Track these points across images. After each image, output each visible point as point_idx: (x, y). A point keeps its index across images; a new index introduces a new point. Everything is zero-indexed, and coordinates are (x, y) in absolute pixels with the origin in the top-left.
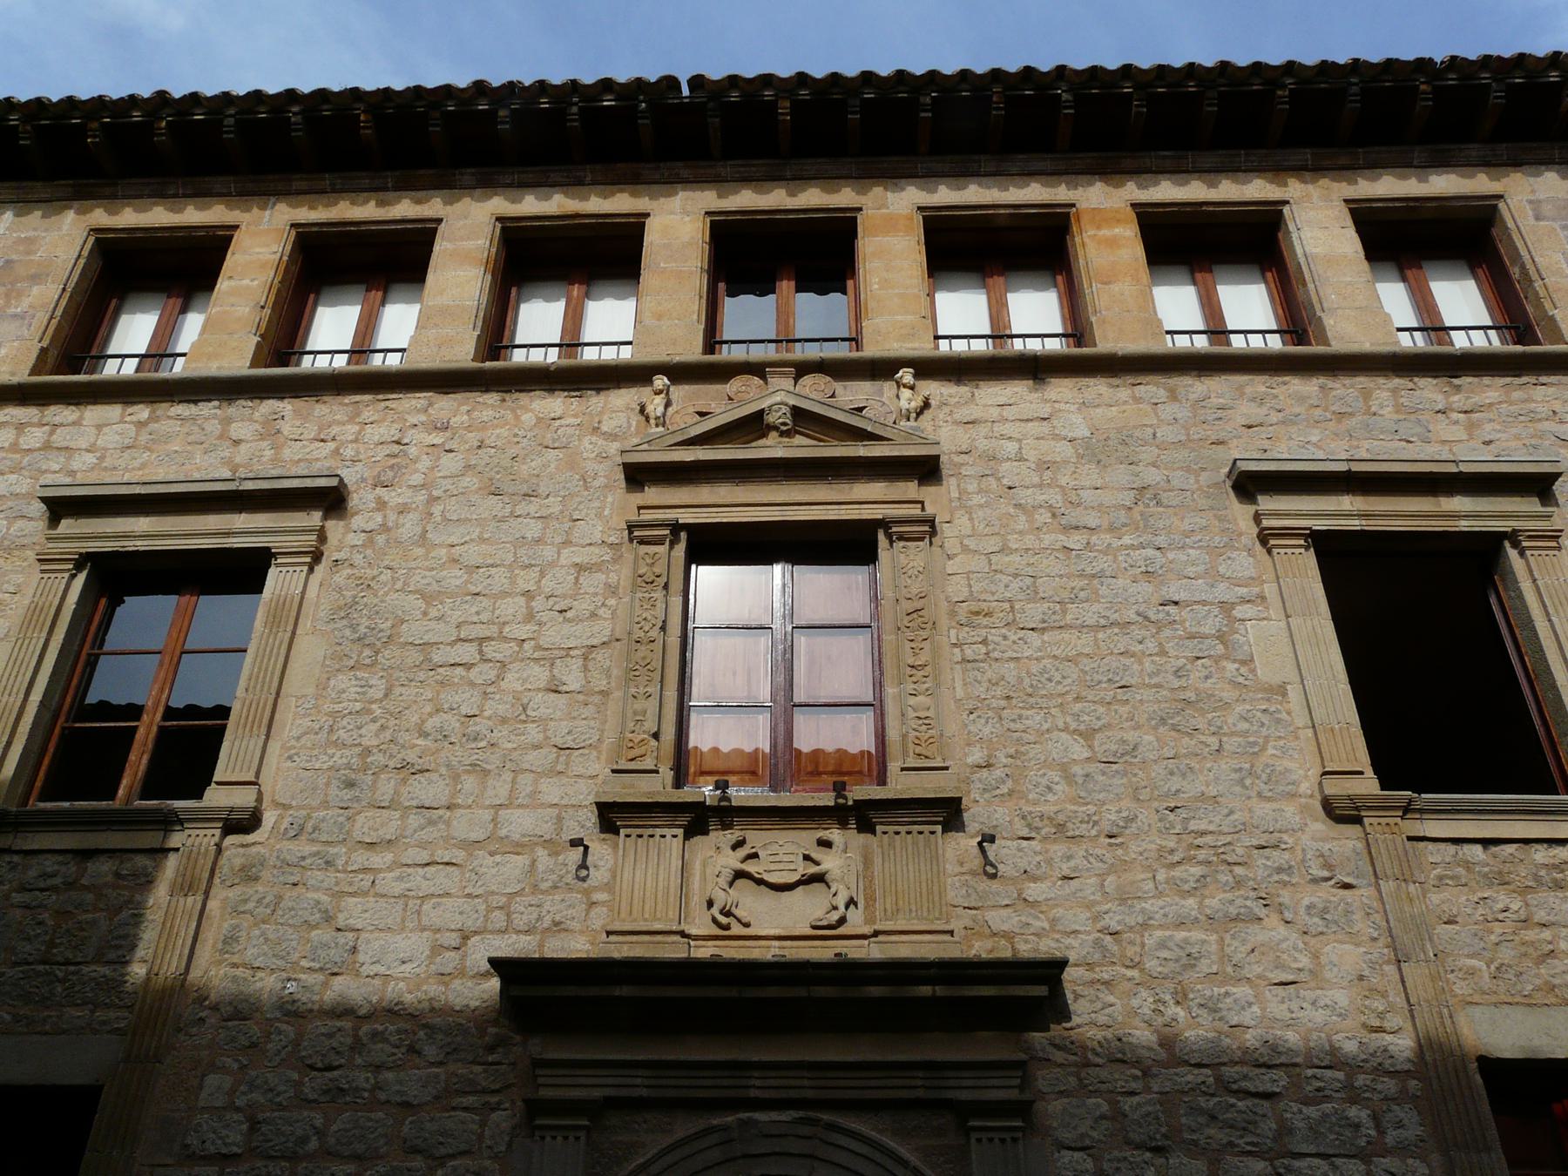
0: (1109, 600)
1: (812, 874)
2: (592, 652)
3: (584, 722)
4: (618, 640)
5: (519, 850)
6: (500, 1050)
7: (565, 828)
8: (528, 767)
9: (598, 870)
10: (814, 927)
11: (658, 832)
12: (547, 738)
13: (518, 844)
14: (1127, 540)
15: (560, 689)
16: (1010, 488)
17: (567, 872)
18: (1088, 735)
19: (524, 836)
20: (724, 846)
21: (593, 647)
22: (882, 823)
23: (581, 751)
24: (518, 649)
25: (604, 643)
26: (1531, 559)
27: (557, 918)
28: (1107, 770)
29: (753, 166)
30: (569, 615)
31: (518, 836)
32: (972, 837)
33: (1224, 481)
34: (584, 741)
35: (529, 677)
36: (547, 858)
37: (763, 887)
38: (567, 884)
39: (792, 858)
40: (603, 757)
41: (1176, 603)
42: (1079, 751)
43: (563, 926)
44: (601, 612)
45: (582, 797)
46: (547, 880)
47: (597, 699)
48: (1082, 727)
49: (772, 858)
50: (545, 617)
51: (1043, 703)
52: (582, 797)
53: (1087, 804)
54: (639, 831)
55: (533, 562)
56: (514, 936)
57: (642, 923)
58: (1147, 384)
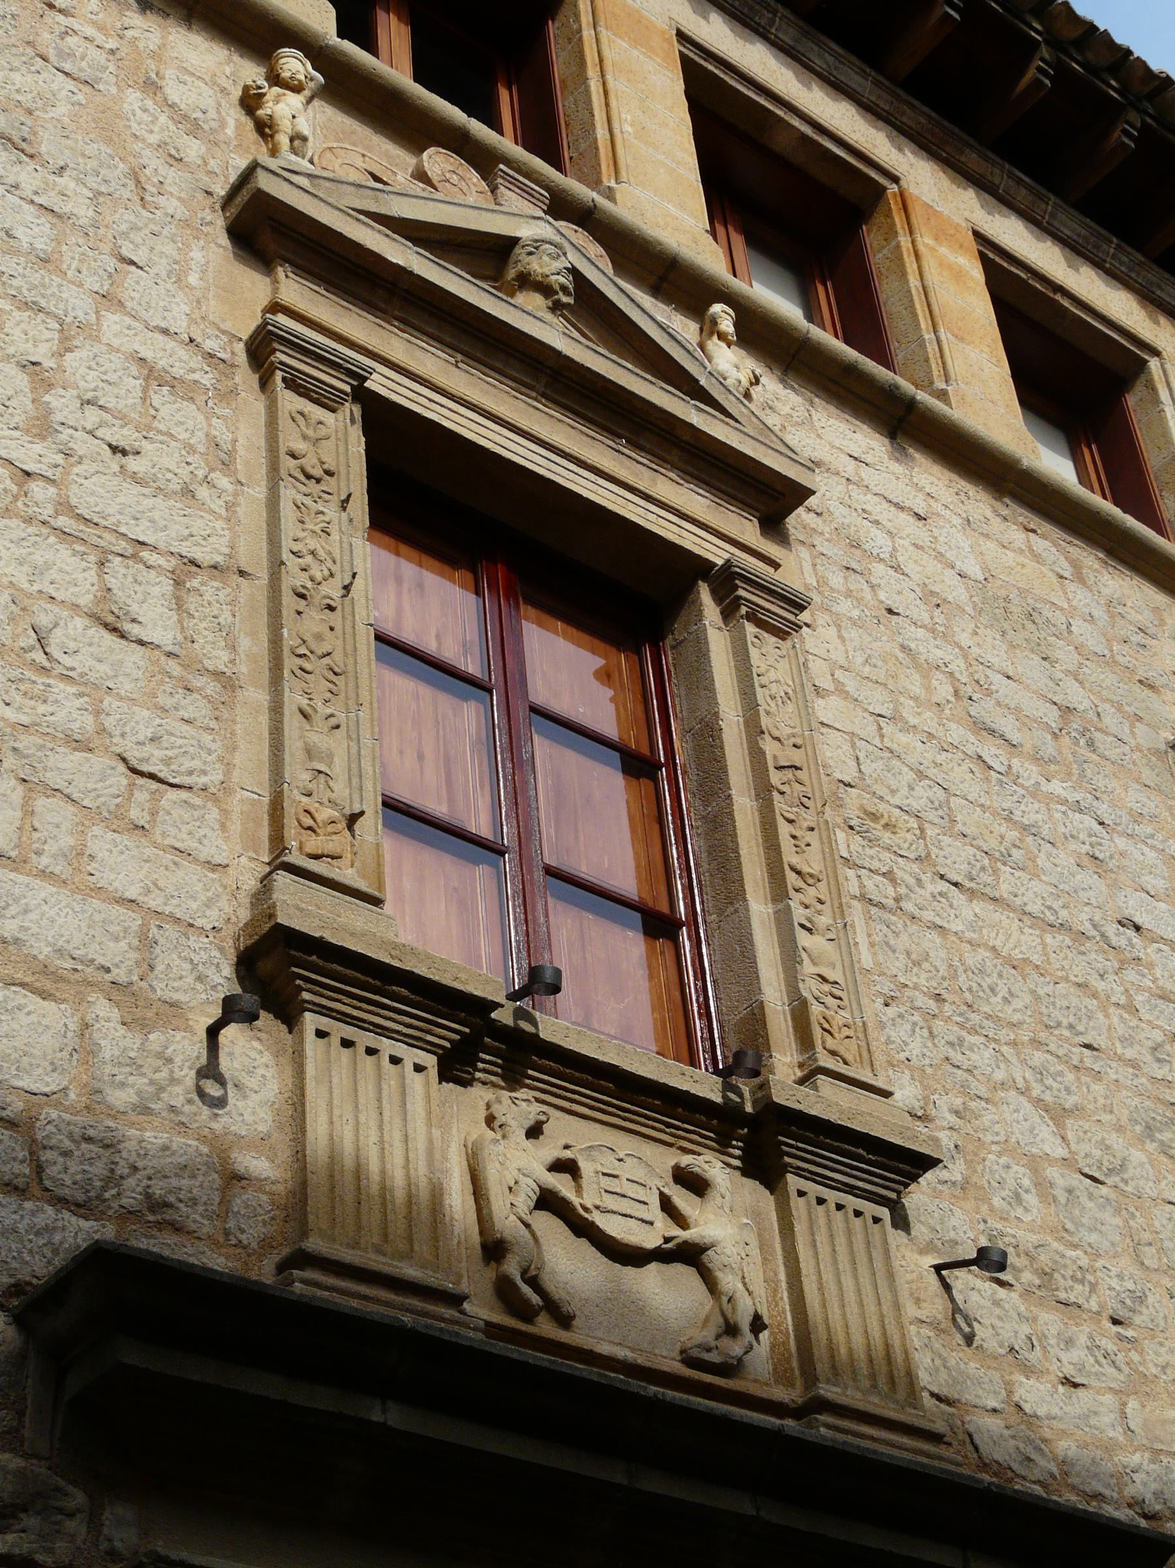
0: (1054, 881)
1: (685, 1242)
2: (191, 575)
3: (186, 728)
4: (242, 573)
5: (49, 986)
6: (31, 1521)
7: (160, 968)
8: (60, 784)
9: (245, 1097)
10: (690, 1361)
11: (388, 1046)
12: (102, 731)
13: (45, 970)
14: (1056, 787)
15: (127, 627)
16: (890, 611)
17: (173, 1081)
18: (1058, 1114)
19: (59, 951)
20: (513, 1123)
21: (193, 562)
22: (799, 1171)
23: (184, 795)
24: (15, 488)
25: (215, 567)
26: (798, 1206)
27: (157, 1191)
28: (1096, 1192)
29: (913, 107)
30: (132, 463)
31: (47, 950)
32: (921, 1252)
33: (1166, 752)
34: (190, 773)
35: (48, 566)
36: (122, 1030)
37: (584, 1243)
38: (172, 1109)
39: (640, 1194)
40: (235, 827)
41: (1137, 928)
42: (1048, 1143)
43: (169, 1215)
44: (203, 492)
45: (194, 905)
46: (123, 1085)
47: (211, 687)
48: (1048, 1097)
49: (606, 1182)
50: (82, 444)
51: (989, 1027)
52: (194, 905)
53: (1075, 1247)
54: (349, 1032)
55: (43, 303)
56: (50, 1210)
57: (373, 1256)
58: (1043, 537)
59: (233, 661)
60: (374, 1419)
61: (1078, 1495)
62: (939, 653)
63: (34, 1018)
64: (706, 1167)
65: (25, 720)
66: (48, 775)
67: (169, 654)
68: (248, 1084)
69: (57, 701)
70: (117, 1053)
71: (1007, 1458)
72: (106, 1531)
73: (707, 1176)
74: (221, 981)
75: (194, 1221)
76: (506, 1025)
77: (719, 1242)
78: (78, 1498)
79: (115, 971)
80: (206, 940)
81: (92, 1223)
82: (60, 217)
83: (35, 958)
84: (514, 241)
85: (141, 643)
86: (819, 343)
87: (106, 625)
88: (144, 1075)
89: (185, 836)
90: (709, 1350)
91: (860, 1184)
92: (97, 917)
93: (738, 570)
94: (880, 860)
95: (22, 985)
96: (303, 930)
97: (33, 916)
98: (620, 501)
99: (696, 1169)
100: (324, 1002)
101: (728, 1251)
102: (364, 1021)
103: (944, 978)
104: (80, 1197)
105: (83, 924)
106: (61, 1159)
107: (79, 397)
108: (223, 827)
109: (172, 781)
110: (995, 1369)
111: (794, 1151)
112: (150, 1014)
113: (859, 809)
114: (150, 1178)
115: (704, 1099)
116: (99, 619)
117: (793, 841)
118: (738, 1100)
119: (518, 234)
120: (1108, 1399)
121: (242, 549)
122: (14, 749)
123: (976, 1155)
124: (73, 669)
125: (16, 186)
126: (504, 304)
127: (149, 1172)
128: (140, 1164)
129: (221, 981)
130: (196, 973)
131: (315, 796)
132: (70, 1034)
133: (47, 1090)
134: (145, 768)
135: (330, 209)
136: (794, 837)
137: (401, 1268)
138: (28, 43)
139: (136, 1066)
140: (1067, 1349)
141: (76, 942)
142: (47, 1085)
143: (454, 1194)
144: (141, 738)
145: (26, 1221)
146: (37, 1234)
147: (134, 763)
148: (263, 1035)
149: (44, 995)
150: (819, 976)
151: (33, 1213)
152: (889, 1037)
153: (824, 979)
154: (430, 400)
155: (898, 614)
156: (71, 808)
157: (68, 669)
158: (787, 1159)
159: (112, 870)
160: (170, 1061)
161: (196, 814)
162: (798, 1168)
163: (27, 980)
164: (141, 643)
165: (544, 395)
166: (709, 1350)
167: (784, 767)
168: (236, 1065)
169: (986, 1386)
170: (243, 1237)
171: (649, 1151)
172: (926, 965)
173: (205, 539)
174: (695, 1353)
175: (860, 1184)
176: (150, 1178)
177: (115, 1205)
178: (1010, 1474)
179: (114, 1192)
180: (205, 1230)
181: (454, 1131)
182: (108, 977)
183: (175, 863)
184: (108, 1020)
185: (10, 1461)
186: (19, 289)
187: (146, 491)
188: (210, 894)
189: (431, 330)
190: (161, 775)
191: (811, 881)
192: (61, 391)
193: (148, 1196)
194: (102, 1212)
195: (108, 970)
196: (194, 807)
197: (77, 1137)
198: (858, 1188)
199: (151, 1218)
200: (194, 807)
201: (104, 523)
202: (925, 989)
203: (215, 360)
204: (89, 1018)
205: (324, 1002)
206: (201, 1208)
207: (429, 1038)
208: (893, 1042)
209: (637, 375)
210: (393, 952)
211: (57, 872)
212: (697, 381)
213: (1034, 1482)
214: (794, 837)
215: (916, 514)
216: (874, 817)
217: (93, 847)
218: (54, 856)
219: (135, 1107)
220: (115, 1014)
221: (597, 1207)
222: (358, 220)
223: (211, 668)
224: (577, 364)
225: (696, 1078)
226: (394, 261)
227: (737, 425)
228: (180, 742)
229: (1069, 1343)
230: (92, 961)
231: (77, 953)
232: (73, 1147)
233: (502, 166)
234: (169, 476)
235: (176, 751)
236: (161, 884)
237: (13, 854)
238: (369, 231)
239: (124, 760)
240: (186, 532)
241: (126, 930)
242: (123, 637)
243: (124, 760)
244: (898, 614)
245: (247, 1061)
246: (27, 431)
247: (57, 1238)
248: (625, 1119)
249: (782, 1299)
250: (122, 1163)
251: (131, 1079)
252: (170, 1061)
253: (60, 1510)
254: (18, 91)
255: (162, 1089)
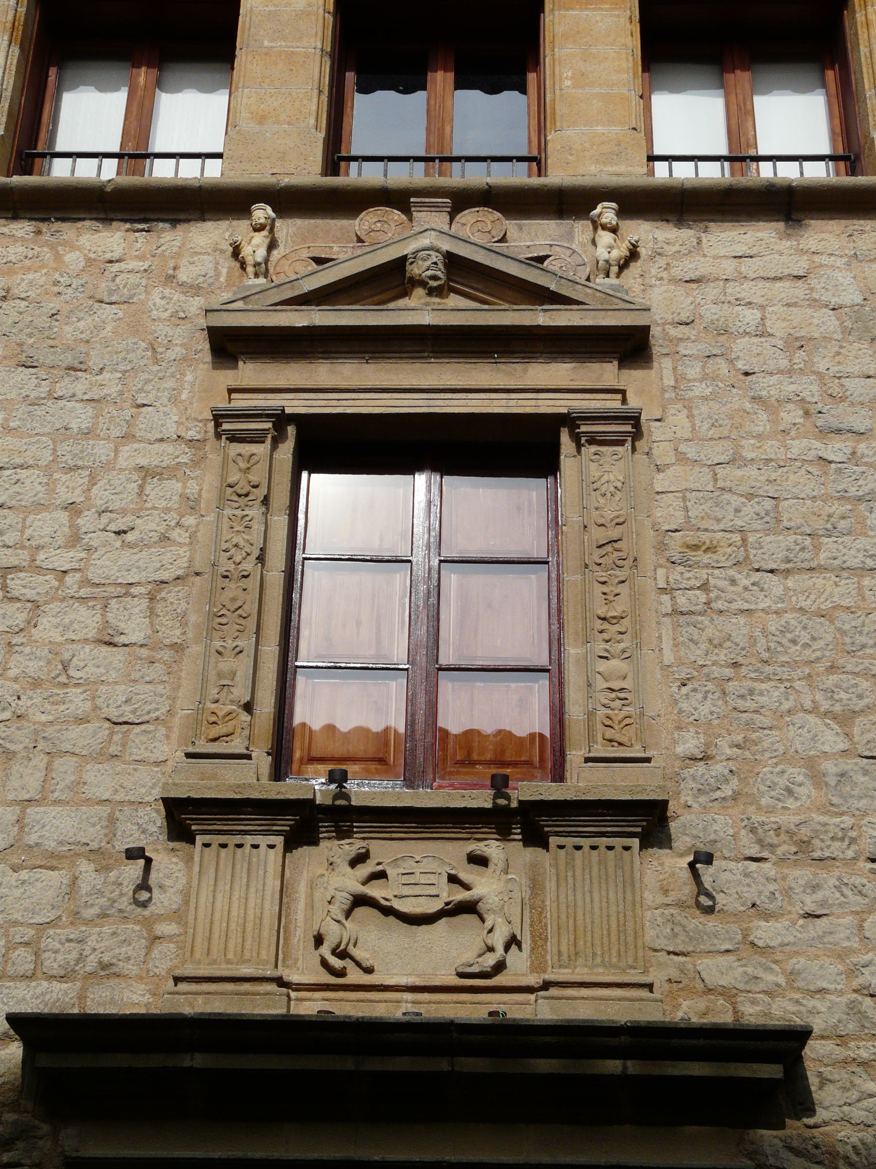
2: (161, 590)
4: (197, 574)
9: (165, 892)
10: (462, 975)
11: (249, 840)
12: (96, 708)
15: (116, 640)
16: (747, 374)
17: (122, 895)
19: (61, 843)
20: (338, 861)
21: (162, 582)
22: (557, 834)
23: (143, 727)
25: (178, 578)
27: (106, 958)
30: (130, 537)
31: (53, 844)
32: (681, 856)
34: (149, 713)
37: (392, 919)
38: (120, 911)
39: (432, 879)
43: (113, 970)
44: (175, 534)
46: (92, 905)
47: (167, 655)
48: (837, 708)
50: (96, 539)
52: (143, 790)
53: (842, 814)
54: (223, 839)
55: (80, 463)
59: (184, 633)
60: (185, 1065)
61: (802, 993)
62: (793, 387)
63: (45, 883)
64: (486, 849)
65: (51, 718)
66: (62, 745)
67: (142, 646)
68: (167, 884)
69: (70, 701)
70: (89, 889)
71: (733, 981)
72: (60, 1143)
73: (485, 854)
74: (156, 829)
75: (128, 969)
76: (328, 805)
77: (484, 897)
78: (46, 1128)
79: (91, 844)
80: (149, 808)
81: (69, 984)
82: (98, 401)
83: (47, 850)
84: (404, 258)
85: (125, 645)
86: (694, 188)
87: (105, 643)
88: (104, 897)
89: (143, 751)
90: (471, 965)
91: (609, 829)
92: (84, 816)
93: (575, 415)
94: (696, 578)
95: (40, 867)
96: (177, 796)
97: (47, 828)
98: (486, 402)
99: (479, 852)
100: (205, 827)
101: (491, 901)
102: (232, 831)
103: (743, 649)
104: (62, 973)
105: (75, 824)
106: (53, 955)
107: (97, 511)
108: (167, 737)
109: (137, 721)
110: (734, 922)
111: (551, 823)
112: (112, 861)
113: (682, 547)
114: (102, 953)
115: (479, 808)
116: (101, 641)
117: (604, 596)
118: (506, 802)
119: (405, 253)
120: (848, 920)
121: (198, 558)
122: (44, 738)
123: (751, 772)
124: (81, 678)
125: (74, 395)
126: (385, 312)
127: (102, 949)
128: (97, 946)
129: (156, 829)
130: (141, 830)
131: (221, 702)
132: (63, 887)
133: (48, 920)
134: (121, 720)
135: (256, 313)
136: (604, 594)
137: (237, 969)
138: (90, 297)
139: (100, 893)
140: (814, 892)
141: (70, 835)
142: (49, 917)
143: (299, 912)
144: (119, 703)
145: (31, 992)
146: (36, 998)
147: (115, 720)
148: (180, 853)
149: (52, 868)
150: (608, 688)
151: (35, 988)
152: (680, 709)
153: (613, 690)
154: (338, 400)
155: (754, 373)
156: (75, 759)
157: (78, 679)
158: (546, 829)
159: (96, 786)
160: (121, 884)
161: (150, 736)
162: (556, 832)
163: (43, 863)
164: (125, 645)
165: (433, 352)
166: (471, 965)
167: (603, 545)
168: (161, 875)
169: (722, 936)
170: (157, 971)
171: (450, 846)
172: (728, 644)
173: (172, 564)
174: (460, 970)
175: (609, 829)
176: (102, 953)
177: (82, 972)
178: (734, 991)
179: (81, 965)
180: (134, 973)
181: (305, 873)
182: (88, 848)
183: (135, 770)
184: (87, 872)
185: (10, 1117)
186: (66, 462)
187: (135, 551)
188: (154, 781)
189: (345, 349)
190: (130, 721)
191: (614, 621)
192: (86, 513)
193: (100, 963)
194: (75, 977)
195: (88, 844)
196: (149, 732)
197: (63, 941)
198: (608, 832)
199: (103, 973)
200: (149, 732)
201: (109, 581)
202: (723, 663)
203: (194, 442)
204: (77, 874)
205: (205, 827)
206: (132, 961)
207: (275, 828)
208: (684, 711)
209: (493, 310)
210: (237, 790)
211: (63, 798)
212: (548, 289)
213: (759, 993)
214: (604, 594)
215: (795, 277)
216: (696, 547)
217: (86, 777)
218: (62, 790)
219: (98, 916)
220: (92, 867)
221: (396, 896)
222: (275, 311)
223: (167, 644)
224: (443, 326)
225: (473, 796)
226: (301, 325)
227: (580, 307)
228: (142, 697)
229: (815, 888)
230: (79, 842)
231: (71, 841)
232: (60, 946)
233: (412, 200)
234: (151, 534)
235: (140, 704)
236: (124, 785)
237: (37, 798)
238: (284, 314)
239: (108, 720)
240: (160, 564)
241: (100, 819)
242: (115, 646)
243: (108, 720)
244: (754, 373)
245: (167, 871)
246: (66, 547)
247: (48, 997)
248: (432, 833)
249: (545, 917)
250: (87, 948)
251: (97, 901)
252: (121, 884)
253: (35, 1137)
254: (82, 333)
255: (114, 901)
